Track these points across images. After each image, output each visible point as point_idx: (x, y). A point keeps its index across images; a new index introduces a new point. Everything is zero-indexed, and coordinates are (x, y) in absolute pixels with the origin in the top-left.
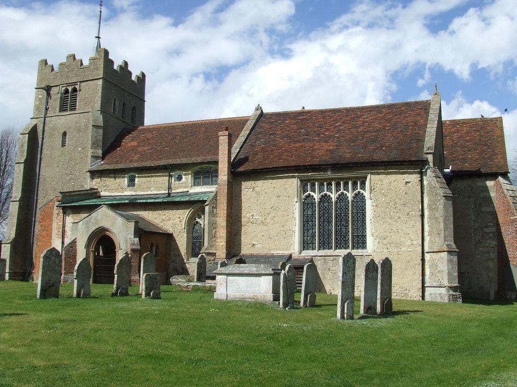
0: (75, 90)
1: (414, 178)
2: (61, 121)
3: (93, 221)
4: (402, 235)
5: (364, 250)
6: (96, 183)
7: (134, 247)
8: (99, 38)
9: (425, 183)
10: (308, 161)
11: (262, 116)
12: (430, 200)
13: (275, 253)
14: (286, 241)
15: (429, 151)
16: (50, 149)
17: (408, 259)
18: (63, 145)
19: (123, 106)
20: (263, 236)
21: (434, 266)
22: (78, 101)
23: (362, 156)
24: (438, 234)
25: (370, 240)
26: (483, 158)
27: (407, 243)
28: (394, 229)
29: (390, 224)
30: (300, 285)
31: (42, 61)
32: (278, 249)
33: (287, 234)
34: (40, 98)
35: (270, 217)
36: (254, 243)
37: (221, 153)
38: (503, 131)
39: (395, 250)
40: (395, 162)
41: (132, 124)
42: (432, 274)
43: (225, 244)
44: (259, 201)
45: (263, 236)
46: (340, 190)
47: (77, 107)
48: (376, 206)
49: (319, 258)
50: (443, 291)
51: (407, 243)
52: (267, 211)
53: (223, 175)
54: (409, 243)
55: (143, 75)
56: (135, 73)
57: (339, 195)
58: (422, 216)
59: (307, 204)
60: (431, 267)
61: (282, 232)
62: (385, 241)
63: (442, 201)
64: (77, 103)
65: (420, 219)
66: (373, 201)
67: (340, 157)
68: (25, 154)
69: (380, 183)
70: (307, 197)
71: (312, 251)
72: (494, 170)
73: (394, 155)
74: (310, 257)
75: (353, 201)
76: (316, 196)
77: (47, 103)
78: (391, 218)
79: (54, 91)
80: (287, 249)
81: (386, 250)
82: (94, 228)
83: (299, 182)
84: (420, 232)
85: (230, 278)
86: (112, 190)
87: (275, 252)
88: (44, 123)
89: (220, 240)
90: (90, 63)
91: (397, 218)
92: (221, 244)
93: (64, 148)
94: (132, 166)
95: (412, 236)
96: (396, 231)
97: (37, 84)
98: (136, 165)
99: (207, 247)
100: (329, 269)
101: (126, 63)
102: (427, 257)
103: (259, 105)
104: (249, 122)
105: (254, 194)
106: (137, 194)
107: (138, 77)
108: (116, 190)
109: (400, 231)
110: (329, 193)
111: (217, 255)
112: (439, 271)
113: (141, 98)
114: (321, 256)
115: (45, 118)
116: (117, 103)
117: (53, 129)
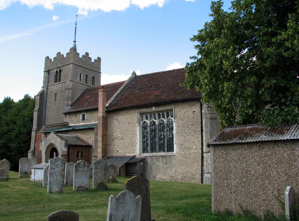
0: (60, 71)
1: (196, 108)
2: (55, 87)
3: (48, 140)
5: (173, 152)
6: (67, 119)
7: (64, 153)
8: (75, 41)
14: (133, 148)
16: (51, 103)
18: (55, 100)
19: (86, 77)
22: (61, 76)
23: (172, 97)
27: (194, 148)
28: (187, 139)
31: (47, 57)
32: (129, 153)
33: (133, 144)
34: (46, 77)
37: (99, 101)
39: (187, 152)
40: (186, 99)
41: (93, 86)
43: (101, 151)
46: (160, 118)
47: (61, 80)
48: (178, 126)
49: (149, 157)
51: (194, 148)
53: (100, 113)
55: (99, 59)
56: (93, 57)
58: (202, 131)
59: (144, 127)
62: (183, 147)
64: (61, 78)
66: (176, 123)
68: (38, 106)
71: (146, 154)
74: (144, 157)
77: (48, 79)
78: (186, 133)
79: (51, 72)
80: (134, 153)
81: (183, 152)
82: (48, 144)
83: (139, 115)
84: (201, 141)
86: (75, 122)
87: (127, 155)
88: (47, 89)
90: (67, 56)
92: (100, 151)
93: (56, 102)
94: (83, 109)
96: (188, 140)
97: (44, 70)
98: (85, 108)
100: (154, 164)
101: (87, 54)
102: (205, 155)
103: (134, 71)
106: (86, 124)
107: (95, 60)
108: (77, 123)
109: (190, 141)
110: (154, 120)
111: (98, 157)
113: (99, 71)
114: (150, 156)
115: (48, 86)
116: (82, 76)
117: (51, 92)
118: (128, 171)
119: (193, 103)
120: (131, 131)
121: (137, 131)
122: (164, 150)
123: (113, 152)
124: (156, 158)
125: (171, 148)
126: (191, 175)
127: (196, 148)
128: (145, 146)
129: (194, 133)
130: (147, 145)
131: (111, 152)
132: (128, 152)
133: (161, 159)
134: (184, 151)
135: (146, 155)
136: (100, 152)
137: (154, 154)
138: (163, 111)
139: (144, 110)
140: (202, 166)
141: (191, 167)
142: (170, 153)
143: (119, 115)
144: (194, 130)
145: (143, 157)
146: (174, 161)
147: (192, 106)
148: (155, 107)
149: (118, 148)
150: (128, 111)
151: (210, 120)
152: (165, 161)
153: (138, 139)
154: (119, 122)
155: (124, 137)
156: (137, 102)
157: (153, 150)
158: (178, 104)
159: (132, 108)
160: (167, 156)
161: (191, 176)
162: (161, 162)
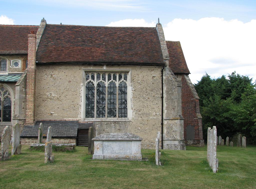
1: (156, 73)
4: (150, 109)
5: (126, 118)
9: (164, 77)
10: (90, 59)
11: (48, 27)
12: (168, 88)
13: (67, 119)
14: (75, 111)
15: (167, 59)
17: (153, 123)
20: (58, 108)
21: (169, 128)
24: (173, 109)
25: (130, 113)
26: (174, 64)
28: (145, 105)
29: (143, 102)
30: (87, 139)
32: (69, 117)
33: (76, 107)
35: (63, 95)
36: (52, 113)
37: (30, 49)
38: (182, 50)
39: (145, 119)
42: (168, 133)
44: (56, 84)
45: (58, 108)
46: (111, 79)
48: (135, 90)
49: (97, 123)
50: (177, 143)
52: (62, 91)
54: (154, 113)
57: (110, 82)
58: (162, 97)
59: (89, 88)
60: (167, 128)
61: (72, 105)
62: (140, 113)
63: (176, 89)
65: (161, 99)
67: (111, 58)
69: (137, 76)
70: (89, 83)
71: (91, 119)
72: (182, 71)
73: (145, 59)
75: (119, 87)
76: (95, 83)
78: (144, 98)
80: (75, 117)
81: (140, 118)
83: (84, 73)
85: (106, 143)
87: (67, 119)
89: (29, 111)
91: (147, 98)
92: (30, 113)
95: (156, 109)
99: (19, 115)
100: (104, 130)
102: (165, 122)
104: (39, 29)
105: (52, 79)
109: (149, 107)
111: (27, 121)
112: (173, 131)
118: (79, 139)
119: (152, 68)
120: (73, 91)
121: (81, 92)
122: (114, 115)
123: (44, 115)
124: (107, 124)
125: (124, 114)
126: (149, 142)
127: (155, 114)
128: (89, 110)
129: (153, 99)
130: (93, 108)
131: (40, 114)
132: (67, 116)
133: (113, 124)
134: (141, 117)
135: (91, 120)
136: (31, 114)
137: (104, 119)
138: (115, 73)
139: (91, 68)
140: (162, 133)
141: (149, 134)
142: (123, 119)
143: (55, 70)
144: (154, 96)
145: (89, 122)
146: (129, 128)
147: (152, 70)
148: (106, 66)
149: (53, 110)
150: (68, 67)
151: (178, 87)
152: (118, 127)
153: (83, 101)
154: (55, 79)
155: (62, 97)
156: (79, 58)
157: (101, 114)
158: (136, 67)
159: (78, 64)
160: (121, 122)
161: (149, 144)
162: (113, 128)
